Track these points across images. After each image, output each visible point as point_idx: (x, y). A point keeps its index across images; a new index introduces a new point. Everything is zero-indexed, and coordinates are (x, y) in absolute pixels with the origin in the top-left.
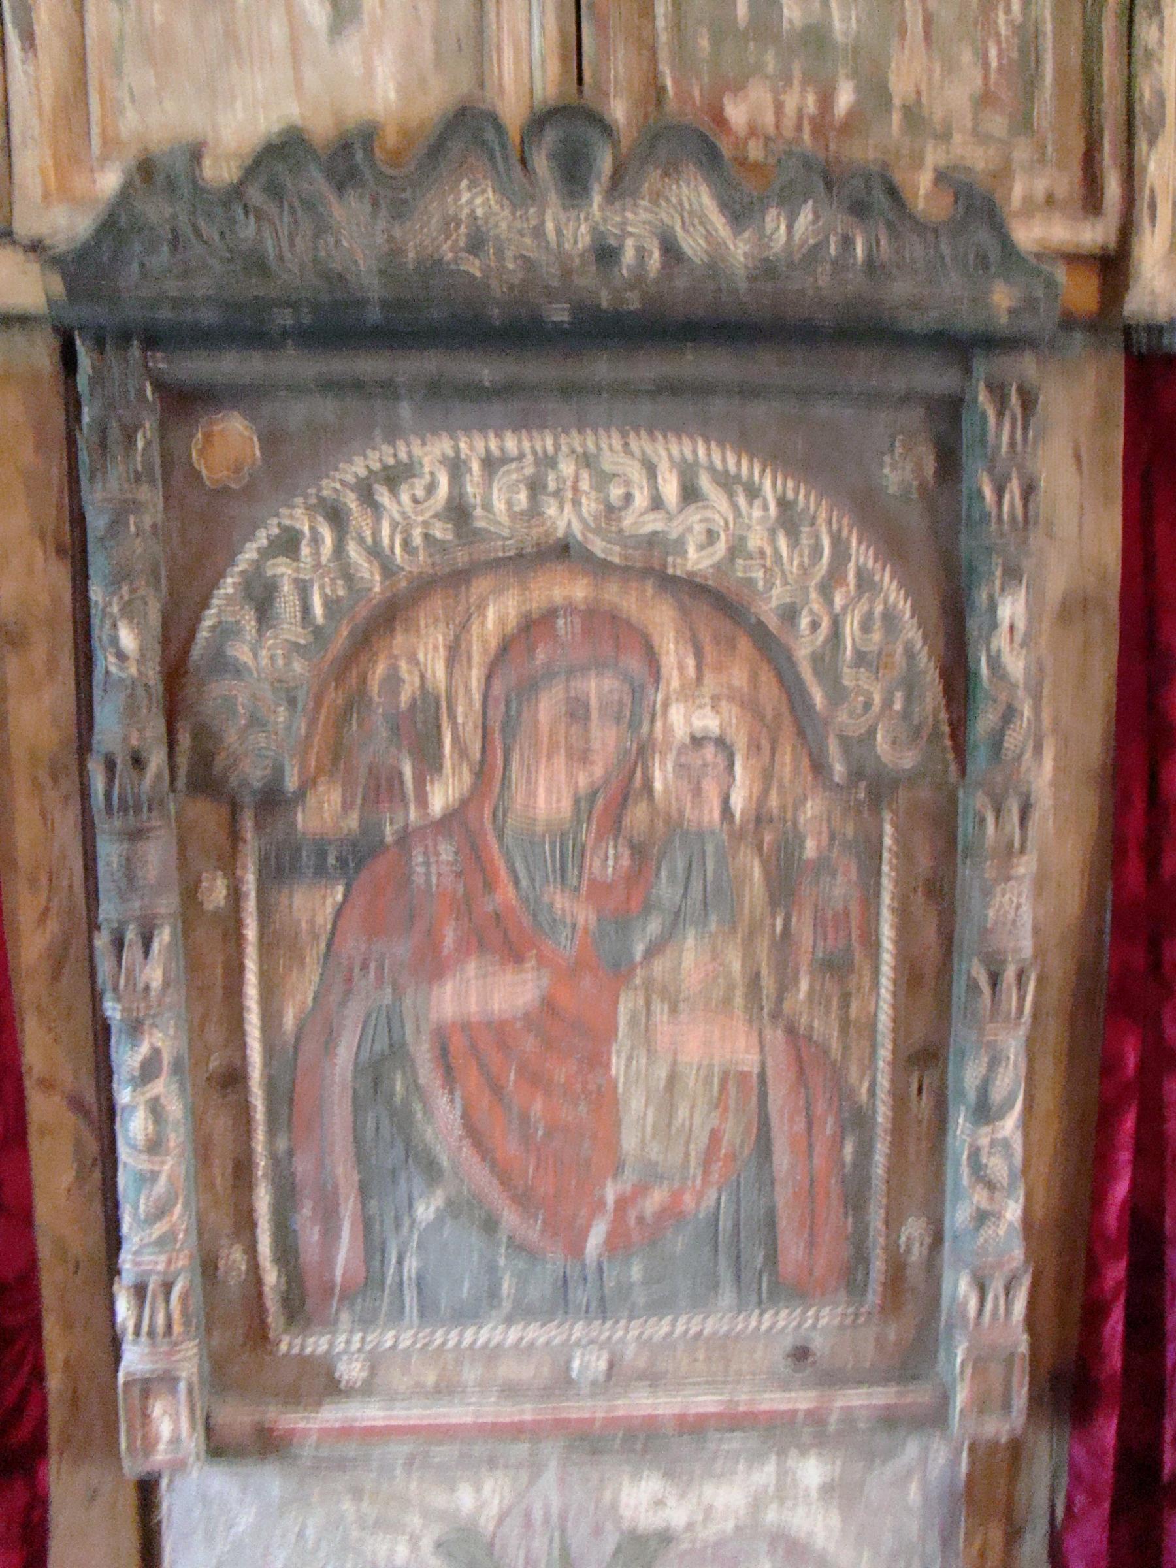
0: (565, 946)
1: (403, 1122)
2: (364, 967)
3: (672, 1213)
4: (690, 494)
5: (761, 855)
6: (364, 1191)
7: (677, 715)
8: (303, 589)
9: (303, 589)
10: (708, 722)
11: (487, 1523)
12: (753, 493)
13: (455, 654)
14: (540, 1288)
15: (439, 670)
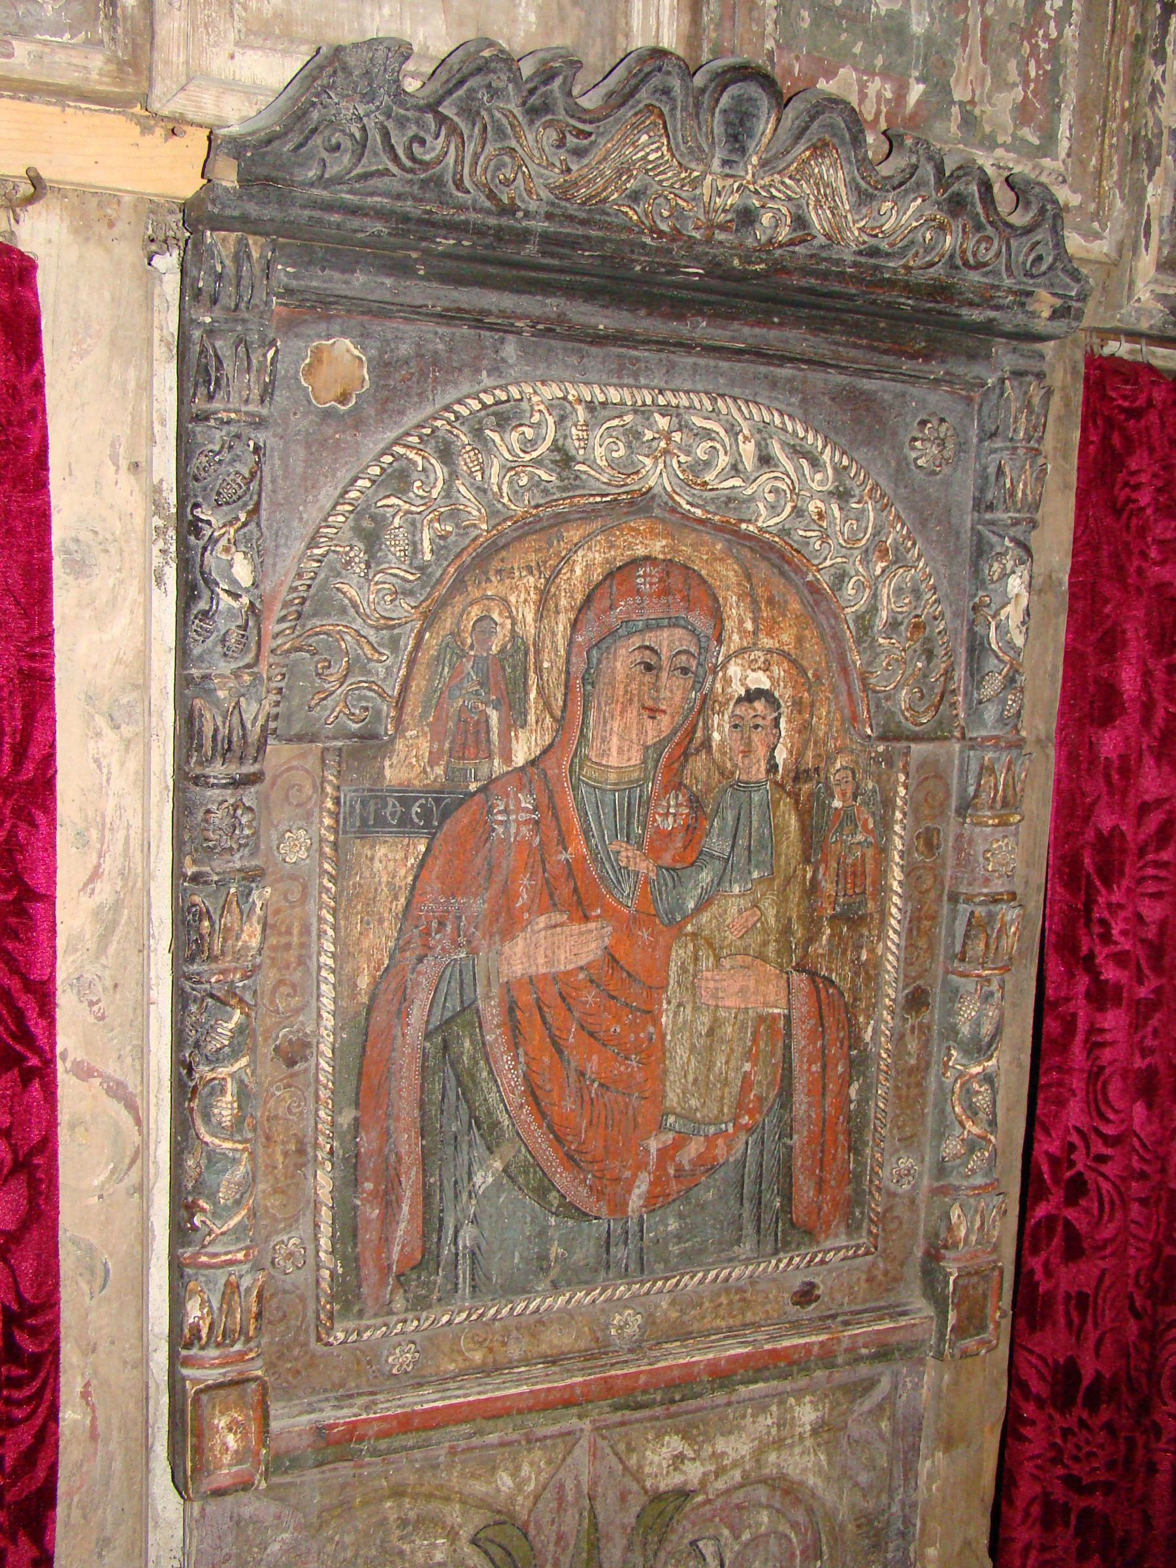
0: (627, 898)
1: (466, 1085)
2: (441, 924)
3: (707, 1165)
4: (765, 460)
5: (797, 809)
6: (426, 1160)
7: (734, 670)
8: (414, 527)
9: (414, 527)
10: (760, 681)
11: (522, 1506)
12: (815, 463)
13: (544, 601)
14: (586, 1251)
15: (529, 614)
